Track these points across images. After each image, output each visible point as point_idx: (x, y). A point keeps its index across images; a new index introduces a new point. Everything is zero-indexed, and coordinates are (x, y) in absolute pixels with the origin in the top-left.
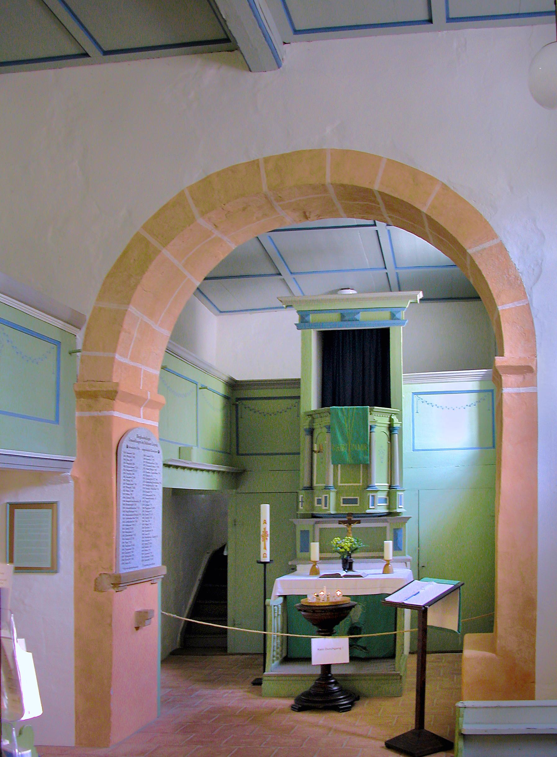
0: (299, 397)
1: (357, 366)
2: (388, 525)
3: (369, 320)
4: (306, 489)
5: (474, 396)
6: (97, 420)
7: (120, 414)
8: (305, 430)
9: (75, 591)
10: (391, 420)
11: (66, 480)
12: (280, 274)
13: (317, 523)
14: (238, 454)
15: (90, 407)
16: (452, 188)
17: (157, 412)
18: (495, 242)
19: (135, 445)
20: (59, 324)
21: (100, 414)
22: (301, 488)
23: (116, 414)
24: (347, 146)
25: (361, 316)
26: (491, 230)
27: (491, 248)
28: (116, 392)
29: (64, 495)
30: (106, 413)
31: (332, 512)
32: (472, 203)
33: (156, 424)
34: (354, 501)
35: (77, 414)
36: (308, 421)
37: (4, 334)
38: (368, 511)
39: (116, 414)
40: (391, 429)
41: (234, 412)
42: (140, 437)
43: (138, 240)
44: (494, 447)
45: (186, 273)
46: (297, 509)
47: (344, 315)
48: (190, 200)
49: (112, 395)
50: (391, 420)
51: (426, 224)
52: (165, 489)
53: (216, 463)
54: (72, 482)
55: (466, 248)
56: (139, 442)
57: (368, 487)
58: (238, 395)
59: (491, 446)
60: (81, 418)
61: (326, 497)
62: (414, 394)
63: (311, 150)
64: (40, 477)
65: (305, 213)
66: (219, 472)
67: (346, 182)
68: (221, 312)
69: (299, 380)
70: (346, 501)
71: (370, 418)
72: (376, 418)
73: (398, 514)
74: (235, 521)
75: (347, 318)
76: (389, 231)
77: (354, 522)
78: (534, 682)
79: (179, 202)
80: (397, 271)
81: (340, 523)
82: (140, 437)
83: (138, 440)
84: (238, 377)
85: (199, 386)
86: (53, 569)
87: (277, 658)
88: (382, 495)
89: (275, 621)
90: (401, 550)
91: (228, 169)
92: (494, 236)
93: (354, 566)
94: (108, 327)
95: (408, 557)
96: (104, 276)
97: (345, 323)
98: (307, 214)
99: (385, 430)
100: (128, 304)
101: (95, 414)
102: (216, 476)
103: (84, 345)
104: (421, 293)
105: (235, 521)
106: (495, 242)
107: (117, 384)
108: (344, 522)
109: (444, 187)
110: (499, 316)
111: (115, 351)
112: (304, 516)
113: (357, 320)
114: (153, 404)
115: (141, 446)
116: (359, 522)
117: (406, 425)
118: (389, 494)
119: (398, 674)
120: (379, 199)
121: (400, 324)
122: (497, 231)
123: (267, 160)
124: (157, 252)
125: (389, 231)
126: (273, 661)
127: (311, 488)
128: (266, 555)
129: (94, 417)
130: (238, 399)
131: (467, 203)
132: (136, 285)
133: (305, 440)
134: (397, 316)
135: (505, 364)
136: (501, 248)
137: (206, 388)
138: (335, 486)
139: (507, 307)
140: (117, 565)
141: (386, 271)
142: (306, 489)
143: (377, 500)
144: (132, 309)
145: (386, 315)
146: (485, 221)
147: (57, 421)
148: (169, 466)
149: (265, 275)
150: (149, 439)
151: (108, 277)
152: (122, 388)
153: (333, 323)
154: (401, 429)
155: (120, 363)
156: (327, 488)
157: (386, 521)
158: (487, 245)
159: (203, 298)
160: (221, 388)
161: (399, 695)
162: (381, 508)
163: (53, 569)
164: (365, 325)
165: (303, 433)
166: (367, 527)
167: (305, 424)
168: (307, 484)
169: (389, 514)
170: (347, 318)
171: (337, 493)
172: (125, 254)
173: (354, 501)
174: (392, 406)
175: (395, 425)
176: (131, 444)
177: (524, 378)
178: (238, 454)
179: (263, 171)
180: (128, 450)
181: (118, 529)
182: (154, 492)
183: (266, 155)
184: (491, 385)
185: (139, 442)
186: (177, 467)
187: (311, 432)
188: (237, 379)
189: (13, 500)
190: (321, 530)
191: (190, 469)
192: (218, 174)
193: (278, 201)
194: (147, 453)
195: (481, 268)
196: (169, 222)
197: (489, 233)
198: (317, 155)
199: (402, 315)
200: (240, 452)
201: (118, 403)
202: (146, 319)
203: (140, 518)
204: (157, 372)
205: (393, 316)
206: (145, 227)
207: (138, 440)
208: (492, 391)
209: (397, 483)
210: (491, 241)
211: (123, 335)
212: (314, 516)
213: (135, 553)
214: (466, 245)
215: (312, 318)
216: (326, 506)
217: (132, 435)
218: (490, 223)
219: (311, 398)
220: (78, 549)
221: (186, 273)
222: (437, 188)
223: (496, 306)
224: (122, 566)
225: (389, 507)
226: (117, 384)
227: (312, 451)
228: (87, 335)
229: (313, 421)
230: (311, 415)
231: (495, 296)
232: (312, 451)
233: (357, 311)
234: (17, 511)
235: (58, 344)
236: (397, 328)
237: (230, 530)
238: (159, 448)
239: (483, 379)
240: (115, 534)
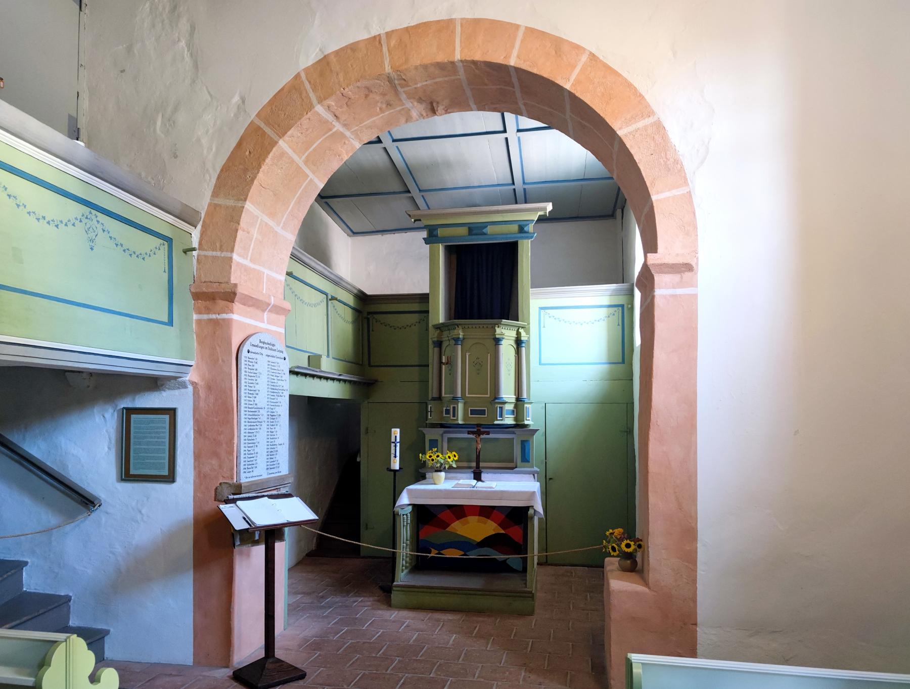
0: (427, 312)
1: (485, 279)
2: (517, 438)
3: (496, 234)
4: (434, 399)
5: (604, 312)
6: (216, 322)
7: (240, 318)
8: (434, 342)
9: (194, 501)
10: (518, 333)
11: (183, 385)
12: (409, 192)
13: (445, 432)
14: (370, 365)
15: (208, 311)
16: (601, 58)
17: (282, 318)
18: (651, 120)
19: (258, 350)
20: (170, 218)
21: (219, 317)
22: (430, 398)
23: (235, 317)
24: (478, 15)
25: (489, 230)
26: (648, 106)
27: (645, 128)
28: (235, 294)
29: (181, 401)
30: (224, 316)
31: (460, 422)
32: (625, 74)
33: (283, 331)
34: (482, 412)
35: (195, 317)
36: (436, 335)
37: (98, 222)
38: (496, 422)
39: (235, 317)
40: (519, 342)
41: (366, 326)
42: (264, 343)
43: (253, 131)
44: (623, 362)
45: (307, 171)
46: (427, 419)
47: (474, 229)
48: (308, 86)
49: (230, 296)
50: (518, 333)
51: (568, 107)
52: (292, 397)
53: (349, 372)
54: (190, 388)
55: (615, 128)
56: (262, 348)
57: (496, 398)
58: (368, 309)
59: (621, 361)
60: (199, 322)
61: (454, 408)
62: (541, 308)
63: (439, 21)
64: (154, 383)
65: (431, 103)
66: (350, 382)
67: (478, 57)
68: (354, 233)
69: (428, 294)
70: (473, 412)
71: (498, 331)
72: (504, 331)
73: (526, 426)
74: (367, 429)
75: (474, 232)
76: (519, 139)
77: (483, 433)
78: (696, 624)
79: (295, 86)
80: (526, 186)
81: (469, 433)
82: (264, 343)
83: (261, 345)
84: (370, 290)
85: (330, 297)
86: (170, 478)
87: (406, 568)
88: (510, 407)
89: (405, 532)
90: (376, 381)
91: (346, 47)
92: (651, 113)
93: (483, 476)
94: (223, 227)
95: (536, 469)
96: (218, 170)
97: (473, 237)
98: (435, 105)
99: (513, 343)
100: (245, 200)
101: (214, 316)
102: (347, 385)
103: (200, 243)
104: (551, 204)
105: (367, 429)
106: (651, 120)
107: (235, 285)
108: (473, 433)
109: (593, 56)
110: (652, 207)
111: (232, 251)
112: (433, 426)
113: (485, 234)
114: (278, 310)
115: (264, 351)
116: (488, 433)
117: (532, 337)
118: (516, 406)
119: (531, 593)
120: (515, 80)
121: (528, 238)
122: (654, 107)
123: (389, 35)
124: (274, 143)
125: (519, 139)
126: (403, 571)
127: (439, 398)
128: (396, 464)
129: (211, 320)
130: (369, 313)
131: (619, 75)
132: (252, 180)
133: (433, 352)
134: (526, 229)
135: (659, 262)
136: (659, 126)
137: (336, 299)
138: (463, 396)
139: (662, 196)
140: (238, 474)
141: (513, 187)
142: (434, 399)
143: (504, 412)
144: (248, 205)
145: (515, 228)
146: (640, 95)
147: (170, 323)
148: (297, 374)
149: (394, 193)
150: (273, 345)
151: (222, 170)
152: (240, 290)
153: (460, 235)
154: (528, 341)
155: (238, 264)
156: (455, 399)
157: (514, 433)
158: (641, 124)
159: (335, 216)
160: (350, 300)
161: (531, 613)
162: (509, 420)
163: (170, 478)
164: (496, 239)
165: (431, 346)
166: (492, 439)
167: (433, 335)
168: (436, 395)
169: (516, 426)
170: (474, 232)
171: (465, 403)
172: (239, 145)
173: (482, 412)
174: (520, 318)
175: (522, 339)
176: (252, 349)
177: (682, 277)
178: (370, 365)
179: (385, 49)
180: (250, 355)
181: (239, 437)
182: (279, 399)
183: (388, 29)
184: (621, 300)
185: (262, 348)
186: (305, 375)
187: (439, 344)
188: (369, 293)
189: (130, 405)
190: (450, 440)
191: (320, 377)
192: (337, 53)
193: (402, 87)
194: (271, 359)
195: (632, 152)
196: (283, 111)
197: (642, 108)
198: (445, 27)
199: (531, 228)
200: (372, 364)
201: (237, 306)
202: (266, 219)
203: (264, 425)
204: (282, 277)
205: (521, 229)
206: (258, 115)
207: (261, 345)
208: (622, 306)
209: (525, 396)
210: (647, 120)
211: (240, 234)
212: (442, 426)
213: (258, 461)
214: (615, 125)
215: (440, 232)
216: (454, 416)
217: (254, 340)
218: (646, 97)
219: (439, 313)
220: (197, 457)
221: (307, 171)
222: (584, 58)
223: (648, 195)
224: (243, 476)
225: (516, 419)
226: (235, 285)
227: (441, 363)
228: (203, 234)
229: (440, 335)
230: (439, 327)
231: (648, 184)
232: (441, 363)
233: (485, 225)
234: (134, 417)
235: (169, 240)
236: (525, 241)
237: (362, 436)
238: (285, 355)
239: (615, 293)
240: (236, 441)
